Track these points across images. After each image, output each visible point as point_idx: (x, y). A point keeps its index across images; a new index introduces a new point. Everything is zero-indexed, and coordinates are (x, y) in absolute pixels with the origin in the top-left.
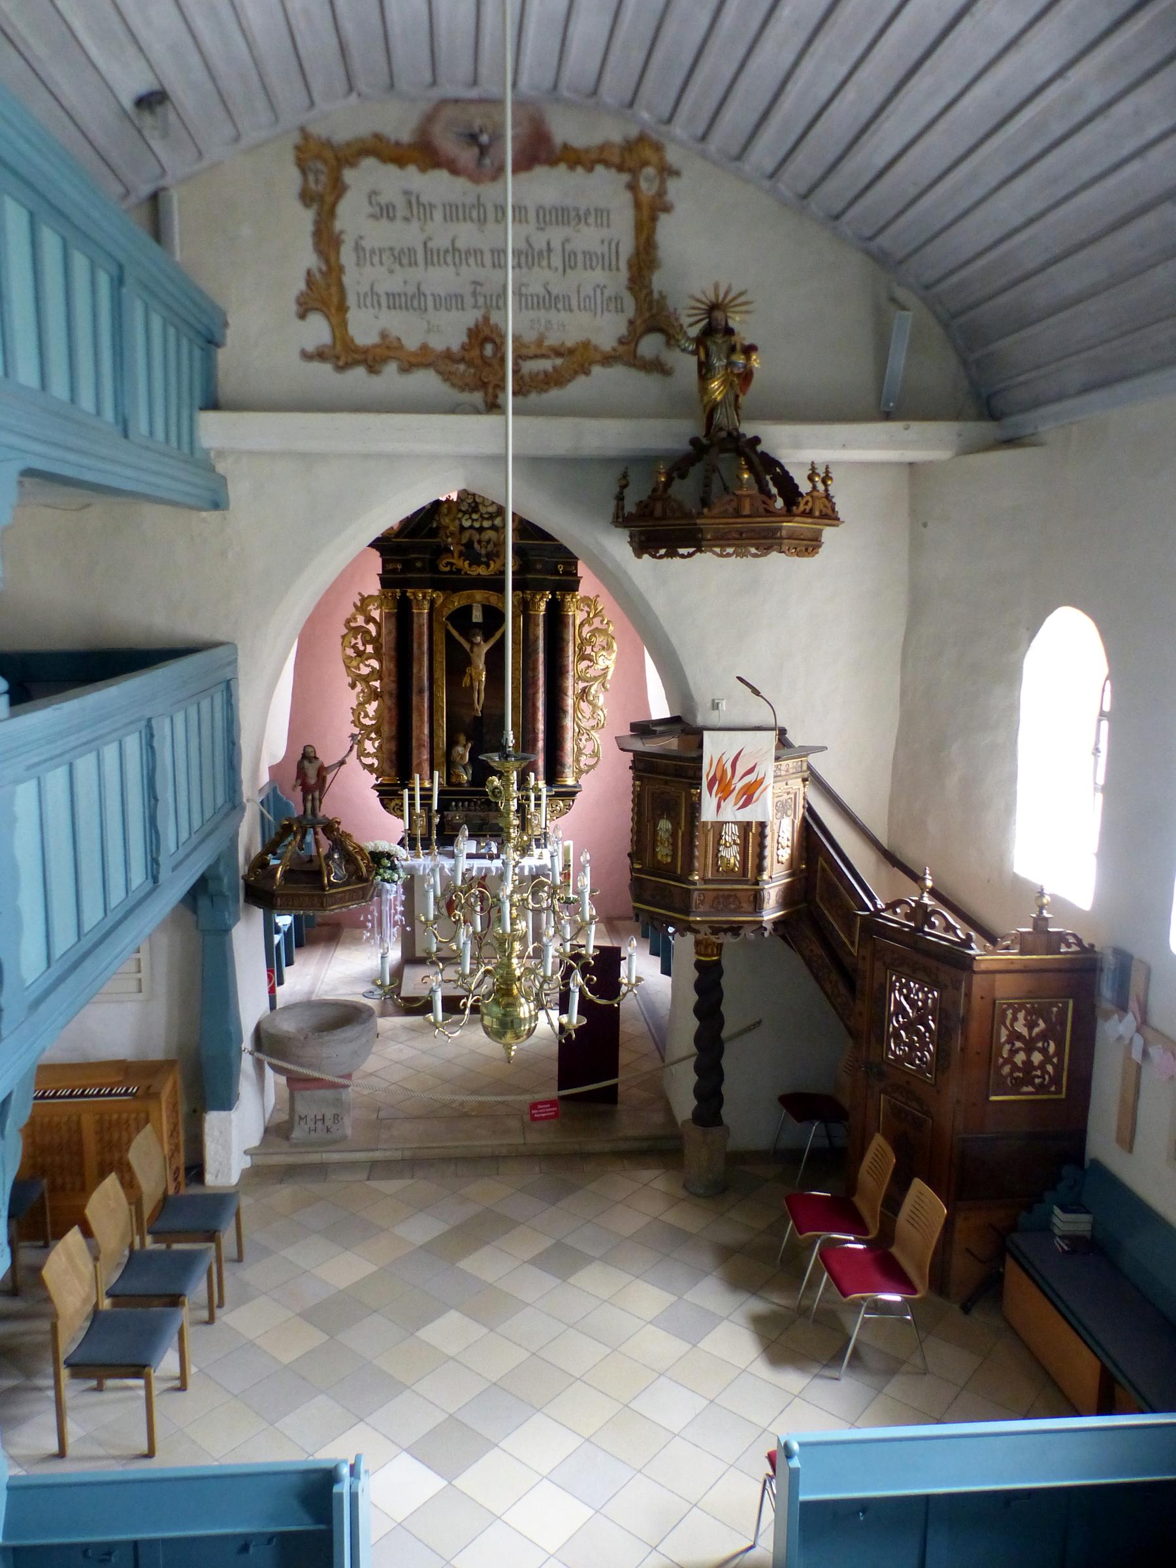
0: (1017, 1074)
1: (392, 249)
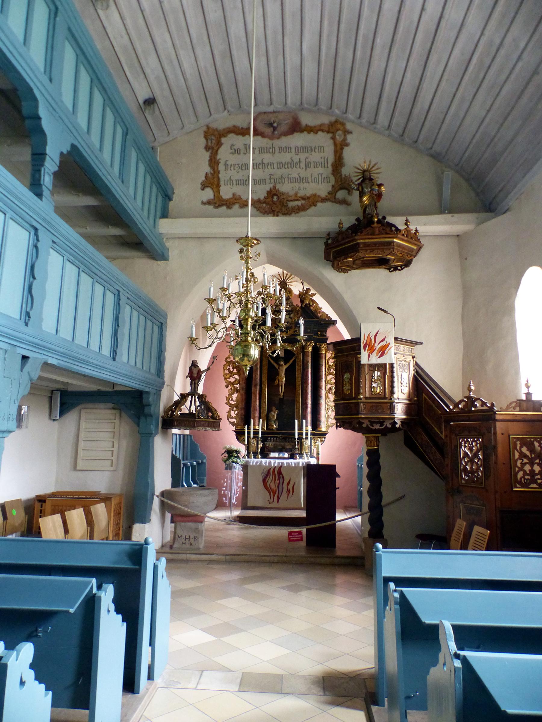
0: (526, 477)
1: (238, 164)
